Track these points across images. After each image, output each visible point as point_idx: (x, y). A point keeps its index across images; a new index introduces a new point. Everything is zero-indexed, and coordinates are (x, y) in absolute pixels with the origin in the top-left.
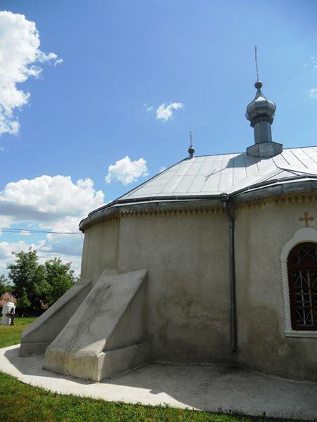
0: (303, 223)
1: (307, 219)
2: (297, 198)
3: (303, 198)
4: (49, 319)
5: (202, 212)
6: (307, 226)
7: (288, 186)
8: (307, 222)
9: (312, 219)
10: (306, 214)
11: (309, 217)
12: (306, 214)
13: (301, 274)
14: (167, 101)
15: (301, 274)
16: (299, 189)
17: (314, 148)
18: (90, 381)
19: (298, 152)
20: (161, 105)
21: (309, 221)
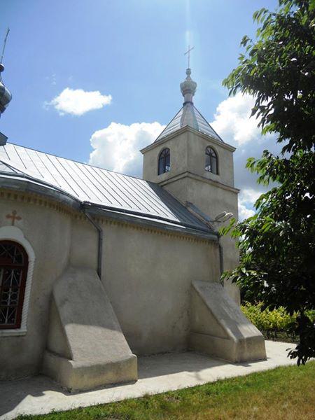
0: (10, 221)
1: (14, 218)
2: (9, 195)
3: (16, 197)
4: (207, 306)
5: (46, 205)
6: (13, 225)
7: (3, 180)
8: (13, 221)
9: (19, 218)
10: (14, 213)
11: (16, 216)
12: (14, 213)
13: (13, 272)
14: (87, 84)
15: (13, 272)
16: (13, 186)
17: (38, 153)
18: (133, 382)
19: (21, 150)
20: (104, 93)
21: (16, 220)
